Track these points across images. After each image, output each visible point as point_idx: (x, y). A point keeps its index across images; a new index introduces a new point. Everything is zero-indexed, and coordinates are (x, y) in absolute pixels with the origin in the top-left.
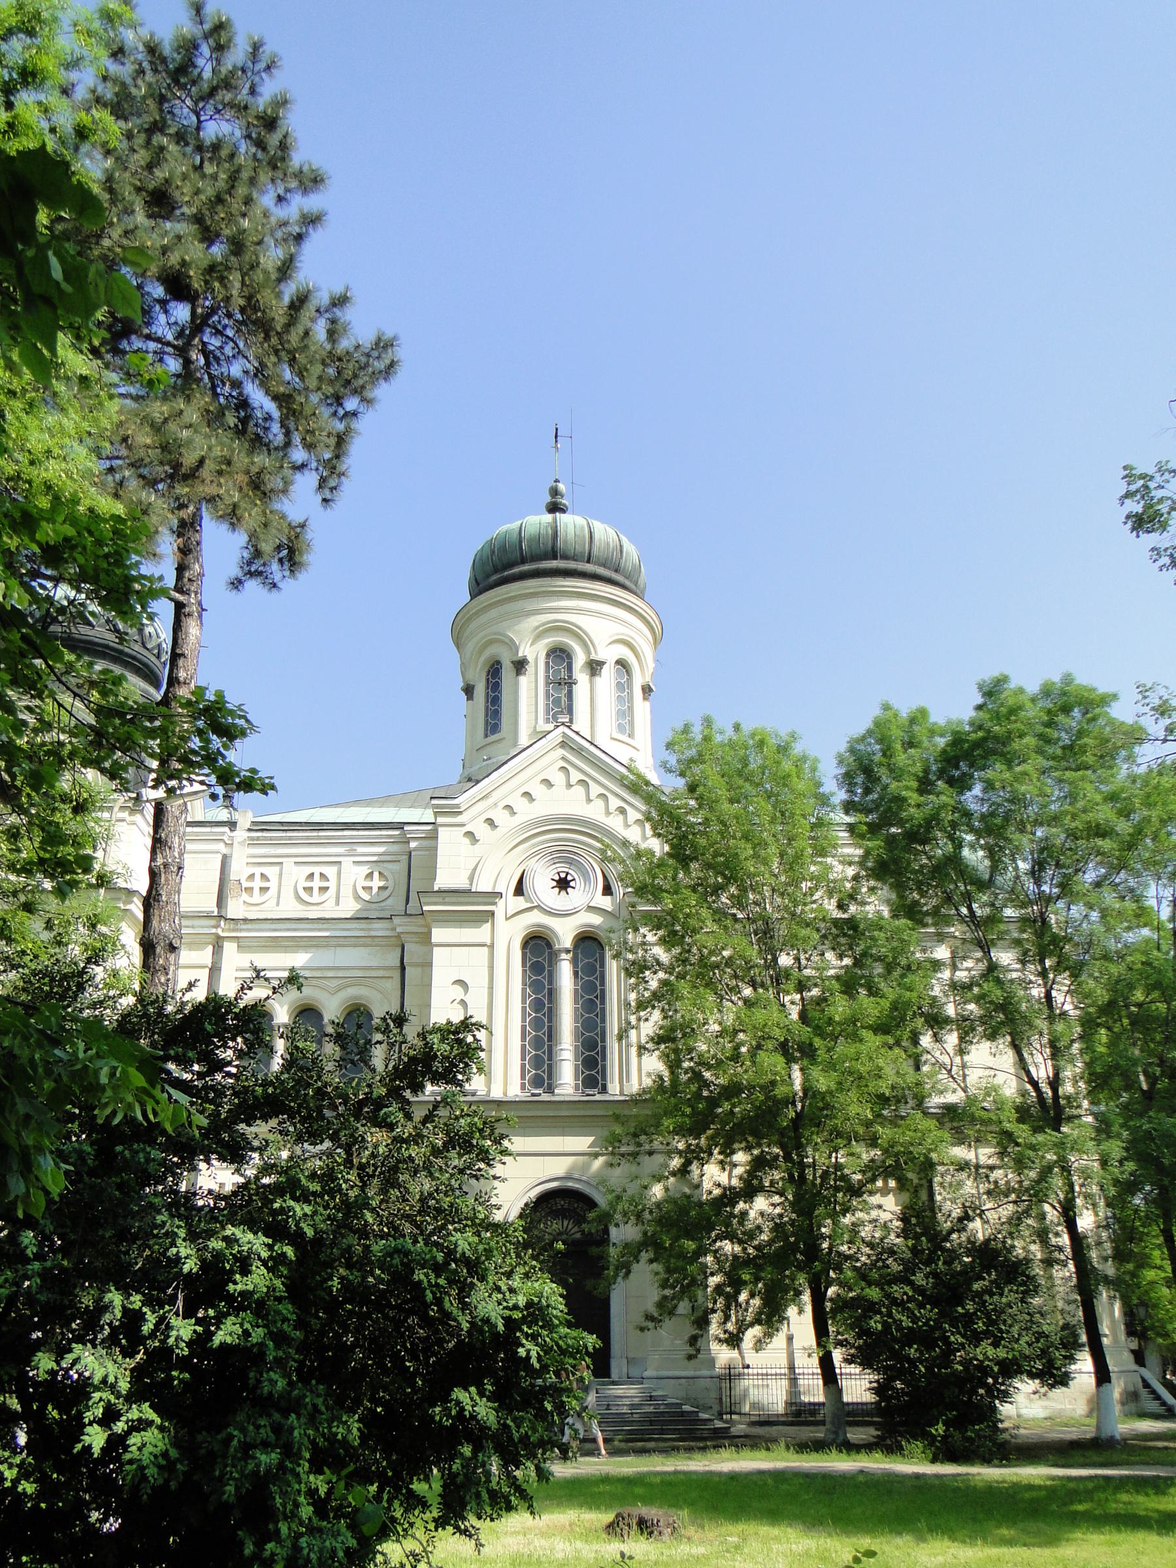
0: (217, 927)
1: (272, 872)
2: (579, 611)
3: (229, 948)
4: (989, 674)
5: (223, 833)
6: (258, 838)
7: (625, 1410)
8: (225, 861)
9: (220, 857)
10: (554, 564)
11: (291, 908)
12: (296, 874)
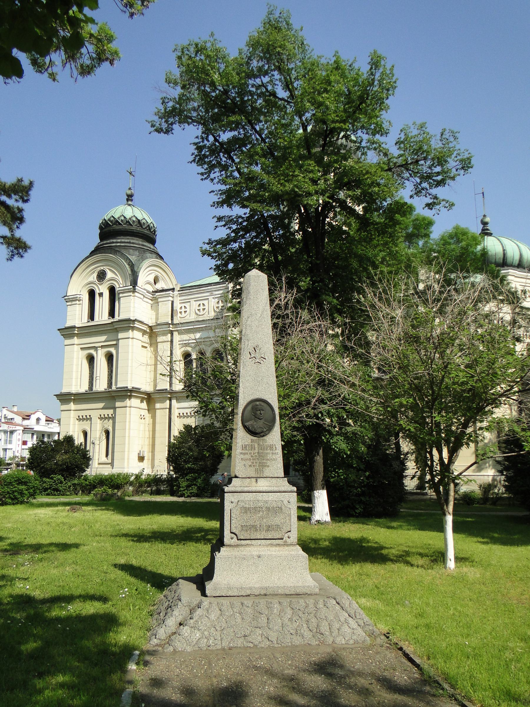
0: (169, 327)
1: (187, 305)
3: (175, 334)
4: (6, 260)
5: (169, 294)
6: (182, 293)
8: (173, 302)
9: (171, 302)
11: (193, 317)
12: (195, 305)
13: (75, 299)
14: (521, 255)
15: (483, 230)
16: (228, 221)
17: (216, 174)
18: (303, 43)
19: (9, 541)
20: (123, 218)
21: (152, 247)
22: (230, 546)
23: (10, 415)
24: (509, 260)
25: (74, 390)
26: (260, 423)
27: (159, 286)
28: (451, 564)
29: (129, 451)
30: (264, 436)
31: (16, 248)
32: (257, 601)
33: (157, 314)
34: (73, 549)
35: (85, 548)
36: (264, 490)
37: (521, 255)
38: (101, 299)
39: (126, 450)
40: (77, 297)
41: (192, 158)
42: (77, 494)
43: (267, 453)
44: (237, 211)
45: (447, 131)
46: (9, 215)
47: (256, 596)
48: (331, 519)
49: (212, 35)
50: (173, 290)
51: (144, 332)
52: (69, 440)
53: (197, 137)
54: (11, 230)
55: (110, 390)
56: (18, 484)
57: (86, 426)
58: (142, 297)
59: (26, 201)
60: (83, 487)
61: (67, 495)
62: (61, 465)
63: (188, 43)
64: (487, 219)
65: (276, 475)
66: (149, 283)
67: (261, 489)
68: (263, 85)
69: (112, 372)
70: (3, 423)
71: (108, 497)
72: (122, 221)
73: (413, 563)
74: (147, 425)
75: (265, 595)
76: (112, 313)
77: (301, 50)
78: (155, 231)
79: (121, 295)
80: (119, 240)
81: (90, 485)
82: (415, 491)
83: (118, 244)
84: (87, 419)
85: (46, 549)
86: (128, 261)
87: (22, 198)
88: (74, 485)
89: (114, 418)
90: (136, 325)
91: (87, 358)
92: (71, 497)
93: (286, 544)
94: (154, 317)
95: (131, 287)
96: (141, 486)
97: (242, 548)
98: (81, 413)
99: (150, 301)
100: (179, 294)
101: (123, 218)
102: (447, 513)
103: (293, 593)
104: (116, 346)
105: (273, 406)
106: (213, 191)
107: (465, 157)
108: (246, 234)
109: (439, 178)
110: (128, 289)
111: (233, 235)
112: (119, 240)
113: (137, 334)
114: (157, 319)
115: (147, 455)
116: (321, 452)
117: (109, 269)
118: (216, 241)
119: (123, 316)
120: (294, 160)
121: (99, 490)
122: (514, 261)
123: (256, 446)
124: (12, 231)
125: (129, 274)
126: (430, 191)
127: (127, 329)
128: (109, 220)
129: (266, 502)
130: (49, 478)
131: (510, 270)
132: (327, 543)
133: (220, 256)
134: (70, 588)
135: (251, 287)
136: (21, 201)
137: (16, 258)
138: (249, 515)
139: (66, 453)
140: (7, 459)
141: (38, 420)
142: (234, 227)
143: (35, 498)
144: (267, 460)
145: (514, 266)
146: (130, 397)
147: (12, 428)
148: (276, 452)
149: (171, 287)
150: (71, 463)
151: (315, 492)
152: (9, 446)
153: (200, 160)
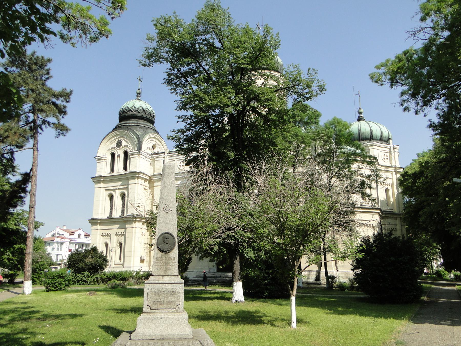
4: (55, 138)
7: (227, 278)
8: (164, 161)
13: (101, 159)
14: (382, 133)
15: (359, 117)
16: (185, 119)
17: (179, 90)
18: (229, 17)
19: (43, 313)
20: (133, 108)
21: (152, 125)
22: (146, 313)
23: (61, 232)
24: (374, 136)
25: (100, 217)
26: (167, 246)
27: (156, 151)
28: (294, 325)
29: (134, 256)
30: (168, 253)
31: (61, 130)
32: (156, 342)
33: (154, 168)
34: (79, 317)
35: (86, 317)
36: (166, 282)
37: (382, 133)
38: (119, 159)
39: (132, 255)
40: (103, 158)
41: (163, 81)
42: (99, 284)
43: (170, 262)
44: (190, 113)
45: (311, 69)
46: (57, 111)
47: (158, 339)
48: (245, 300)
49: (174, 12)
50: (164, 153)
51: (145, 180)
52: (94, 249)
53: (167, 69)
54: (58, 119)
55: (123, 216)
56: (58, 278)
57: (107, 240)
58: (144, 157)
59: (67, 102)
60: (103, 279)
61: (92, 285)
62: (89, 265)
63: (160, 17)
64: (362, 110)
65: (174, 274)
66: (150, 149)
67: (165, 282)
68: (206, 40)
69: (124, 205)
70: (56, 237)
71: (116, 286)
73: (275, 325)
74: (146, 239)
75: (163, 339)
76: (125, 168)
77: (228, 21)
78: (154, 116)
79: (131, 156)
80: (131, 122)
81: (107, 278)
82: (313, 282)
84: (108, 235)
85: (62, 317)
86: (136, 135)
87: (65, 99)
88: (97, 278)
89: (125, 235)
90: (140, 175)
91: (109, 196)
92: (94, 286)
93: (177, 312)
94: (152, 170)
95: (138, 151)
96: (139, 279)
97: (152, 314)
98: (104, 232)
99: (150, 160)
100: (168, 156)
101: (133, 108)
102: (292, 295)
103: (178, 338)
104: (127, 189)
105: (174, 235)
106: (176, 101)
107: (322, 84)
108: (196, 126)
109: (308, 96)
110: (136, 153)
111: (188, 126)
112: (131, 122)
113: (140, 181)
114: (154, 171)
115: (146, 259)
116: (238, 258)
117: (124, 140)
118: (178, 130)
119: (132, 170)
120: (219, 86)
121: (111, 282)
122: (378, 135)
123: (164, 258)
124: (59, 121)
125: (137, 143)
126: (303, 103)
127: (134, 178)
128: (125, 109)
129: (167, 289)
130: (81, 274)
131: (374, 143)
132: (233, 314)
133: (179, 140)
134: (67, 338)
135: (166, 172)
136: (65, 101)
137: (61, 136)
138: (157, 296)
139: (92, 257)
140: (58, 261)
141: (80, 235)
142: (189, 122)
143: (69, 287)
144: (170, 266)
145: (378, 140)
146: (135, 221)
147: (62, 240)
148: (175, 261)
149: (164, 151)
150: (95, 264)
151: (234, 283)
152: (60, 252)
153: (169, 82)
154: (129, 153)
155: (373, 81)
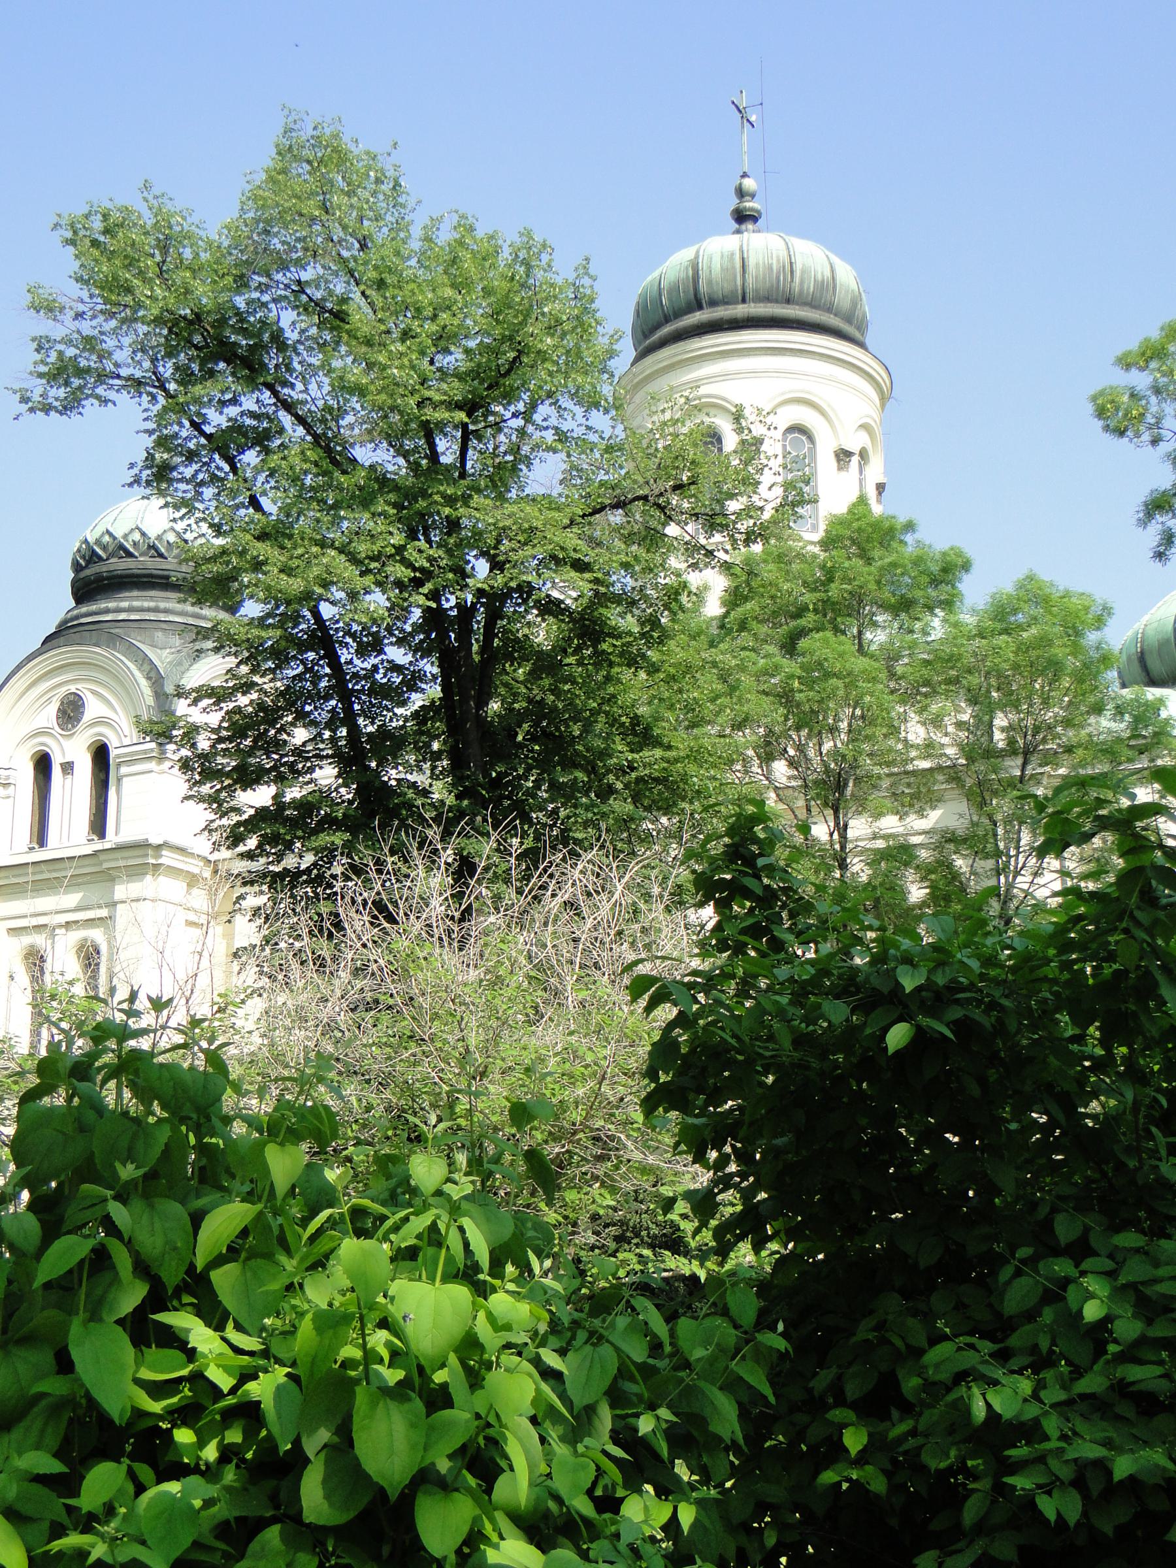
2: (725, 376)
10: (698, 317)
18: (397, 184)
20: (137, 536)
49: (147, 186)
51: (193, 880)
72: (135, 544)
76: (99, 826)
79: (124, 770)
80: (125, 604)
83: (122, 616)
86: (146, 667)
101: (137, 536)
110: (145, 751)
112: (125, 604)
117: (94, 692)
127: (138, 872)
128: (98, 542)
154: (113, 753)
155: (1107, 428)
